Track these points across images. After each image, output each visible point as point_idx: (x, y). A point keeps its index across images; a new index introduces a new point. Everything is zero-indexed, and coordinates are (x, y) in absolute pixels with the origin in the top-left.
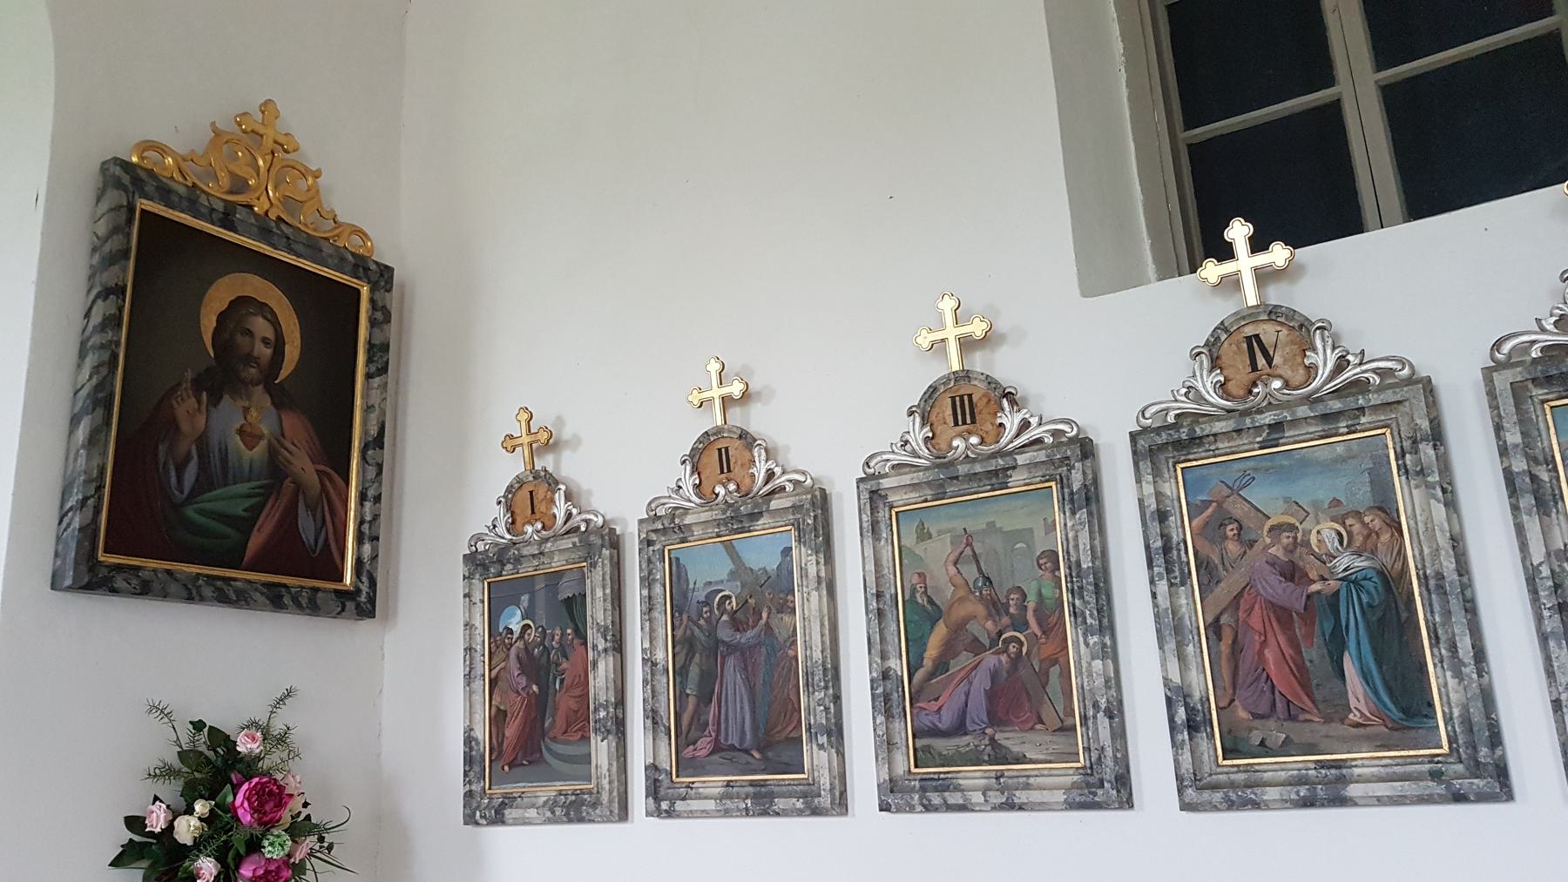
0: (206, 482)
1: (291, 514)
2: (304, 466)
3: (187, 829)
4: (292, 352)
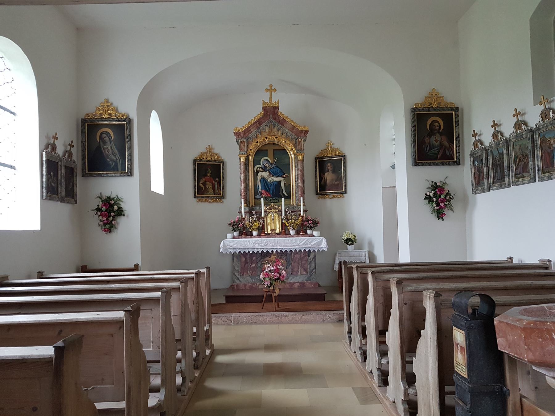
0: (430, 149)
1: (445, 151)
2: (446, 143)
3: (431, 195)
4: (442, 127)
